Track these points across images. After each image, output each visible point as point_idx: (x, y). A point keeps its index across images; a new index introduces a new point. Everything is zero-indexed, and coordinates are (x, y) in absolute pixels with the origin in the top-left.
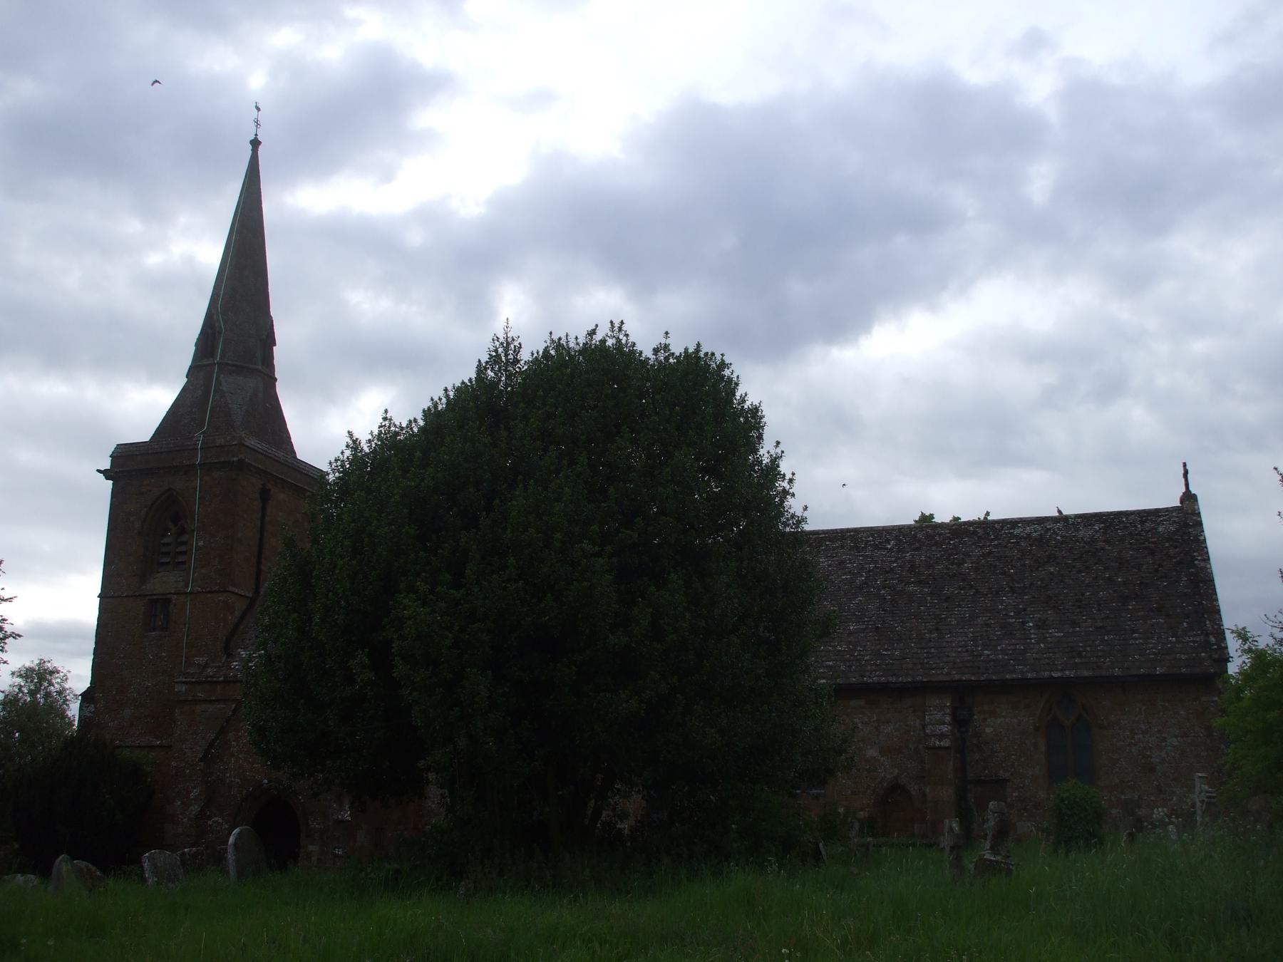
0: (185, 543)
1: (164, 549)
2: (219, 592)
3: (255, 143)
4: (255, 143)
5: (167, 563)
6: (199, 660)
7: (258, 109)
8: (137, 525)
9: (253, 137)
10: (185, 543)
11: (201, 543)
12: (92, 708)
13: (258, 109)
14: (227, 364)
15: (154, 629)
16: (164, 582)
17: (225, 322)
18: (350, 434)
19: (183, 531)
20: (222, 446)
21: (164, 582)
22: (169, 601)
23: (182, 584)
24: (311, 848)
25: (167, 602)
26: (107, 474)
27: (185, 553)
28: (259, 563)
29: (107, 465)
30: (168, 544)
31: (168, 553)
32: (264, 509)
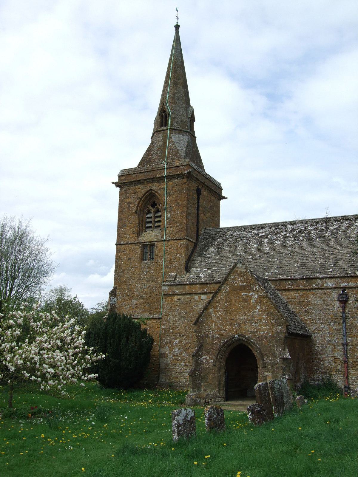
0: (160, 217)
1: (148, 220)
2: (180, 239)
3: (177, 27)
4: (177, 27)
5: (151, 227)
6: (173, 274)
7: (177, 11)
8: (134, 208)
9: (176, 24)
10: (160, 217)
11: (169, 216)
12: (115, 299)
13: (177, 11)
14: (174, 129)
15: (146, 260)
16: (149, 236)
17: (171, 109)
18: (113, 183)
19: (158, 211)
20: (177, 167)
21: (149, 236)
22: (153, 245)
23: (160, 237)
24: (266, 374)
25: (153, 245)
26: (117, 184)
27: (159, 221)
28: (197, 225)
29: (116, 180)
30: (151, 218)
31: (150, 222)
32: (198, 198)
